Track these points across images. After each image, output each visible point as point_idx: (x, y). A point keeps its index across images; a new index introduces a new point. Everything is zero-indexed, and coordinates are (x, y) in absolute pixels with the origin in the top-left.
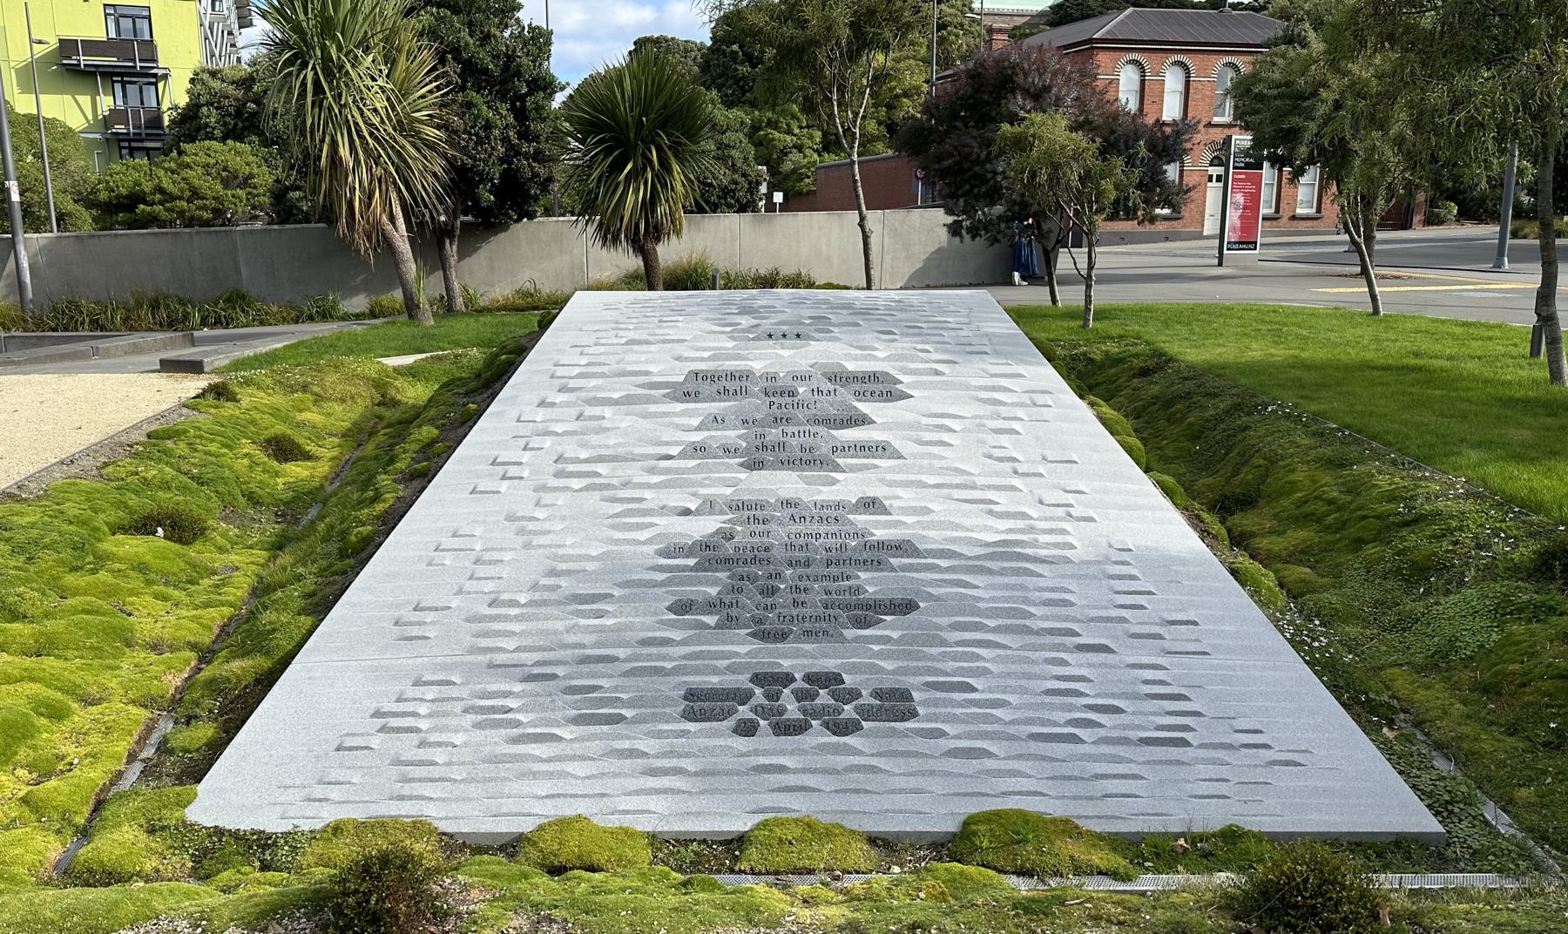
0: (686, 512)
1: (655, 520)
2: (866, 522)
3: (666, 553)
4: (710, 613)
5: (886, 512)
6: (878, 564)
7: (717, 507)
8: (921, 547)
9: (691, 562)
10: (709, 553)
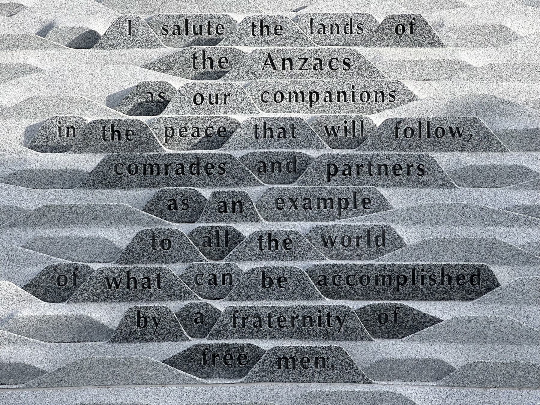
0: (88, 40)
1: (32, 57)
2: (399, 64)
3: (41, 140)
4: (109, 298)
5: (433, 41)
6: (419, 173)
7: (141, 33)
8: (494, 124)
9: (87, 162)
10: (123, 151)
